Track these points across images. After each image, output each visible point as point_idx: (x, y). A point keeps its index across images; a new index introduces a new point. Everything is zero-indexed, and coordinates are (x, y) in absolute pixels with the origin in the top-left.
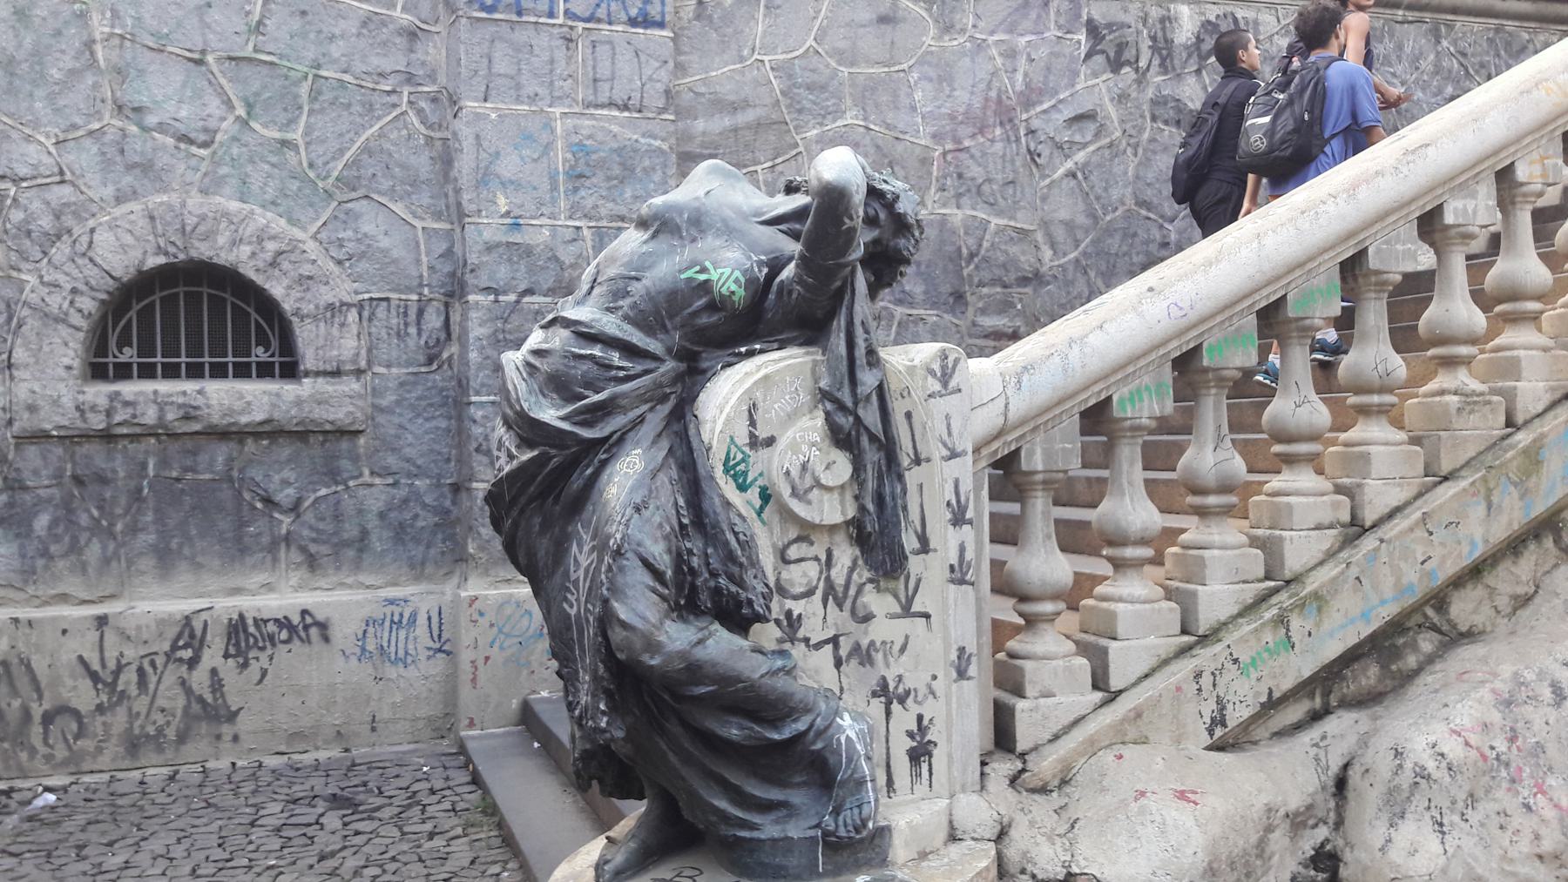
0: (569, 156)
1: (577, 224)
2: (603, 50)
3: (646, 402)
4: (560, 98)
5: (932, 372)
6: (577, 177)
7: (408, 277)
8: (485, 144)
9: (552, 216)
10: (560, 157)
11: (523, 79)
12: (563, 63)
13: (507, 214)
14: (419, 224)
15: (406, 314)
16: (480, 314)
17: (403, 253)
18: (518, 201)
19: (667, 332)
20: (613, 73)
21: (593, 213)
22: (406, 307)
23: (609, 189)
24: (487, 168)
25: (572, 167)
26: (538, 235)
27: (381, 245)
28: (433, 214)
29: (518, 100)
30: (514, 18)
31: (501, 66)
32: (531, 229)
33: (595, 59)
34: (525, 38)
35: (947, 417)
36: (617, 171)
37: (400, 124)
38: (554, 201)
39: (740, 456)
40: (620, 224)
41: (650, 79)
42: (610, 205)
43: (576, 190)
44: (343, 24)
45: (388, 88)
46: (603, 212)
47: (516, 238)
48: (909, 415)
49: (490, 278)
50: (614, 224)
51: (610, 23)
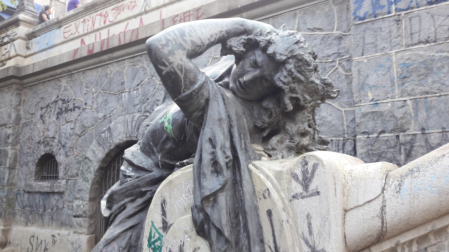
0: (399, 70)
1: (405, 99)
2: (415, 21)
3: (128, 197)
4: (395, 46)
5: (295, 176)
6: (403, 78)
7: (339, 131)
8: (362, 73)
9: (393, 97)
10: (395, 71)
11: (378, 43)
12: (395, 31)
13: (373, 99)
14: (343, 110)
15: (338, 146)
16: (361, 144)
17: (337, 122)
18: (377, 94)
19: (155, 155)
20: (420, 28)
21: (412, 93)
22: (339, 142)
23: (420, 80)
24: (363, 82)
25: (401, 74)
26: (385, 107)
27: (328, 120)
28: (348, 105)
29: (376, 51)
30: (373, 19)
31: (369, 40)
32: (383, 104)
33: (411, 26)
34: (378, 26)
35: (308, 217)
36: (423, 71)
37: (335, 73)
38: (393, 91)
39: (157, 236)
40: (426, 96)
41: (440, 26)
42: (421, 88)
43: (403, 84)
44: (315, 42)
45: (331, 60)
46: (417, 91)
47: (376, 109)
48: (269, 213)
49: (365, 128)
50: (423, 96)
51: (418, 7)
